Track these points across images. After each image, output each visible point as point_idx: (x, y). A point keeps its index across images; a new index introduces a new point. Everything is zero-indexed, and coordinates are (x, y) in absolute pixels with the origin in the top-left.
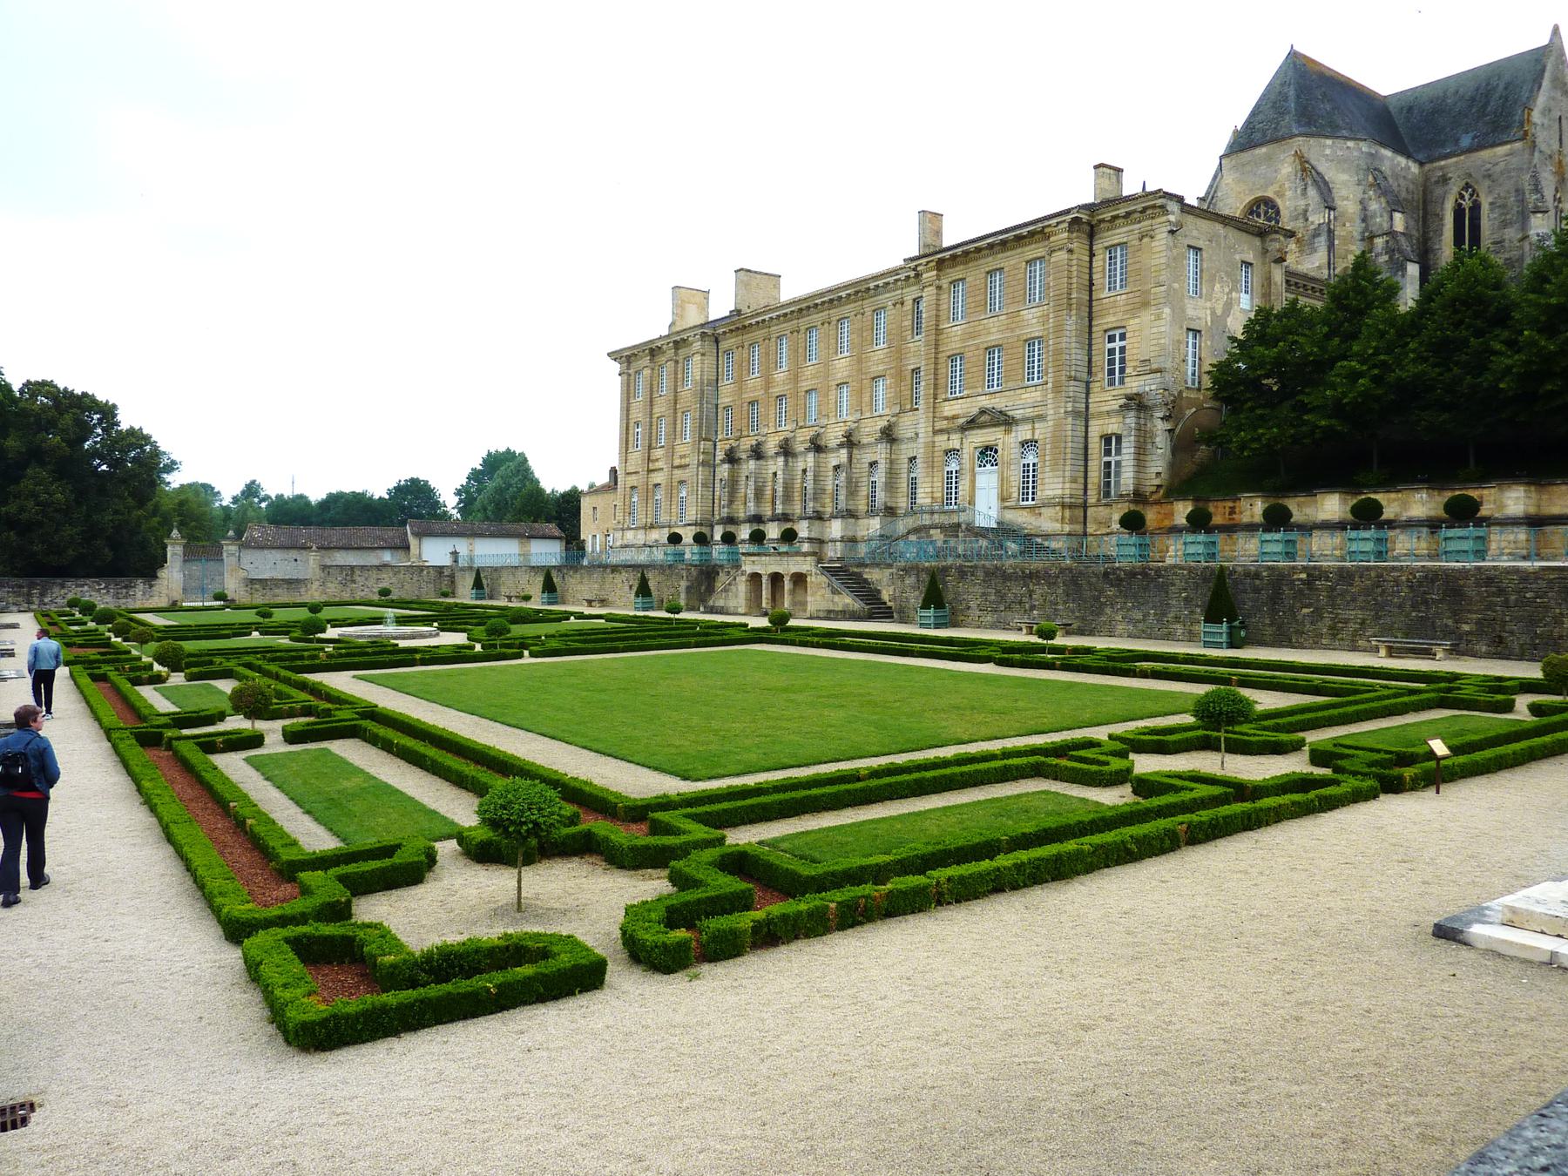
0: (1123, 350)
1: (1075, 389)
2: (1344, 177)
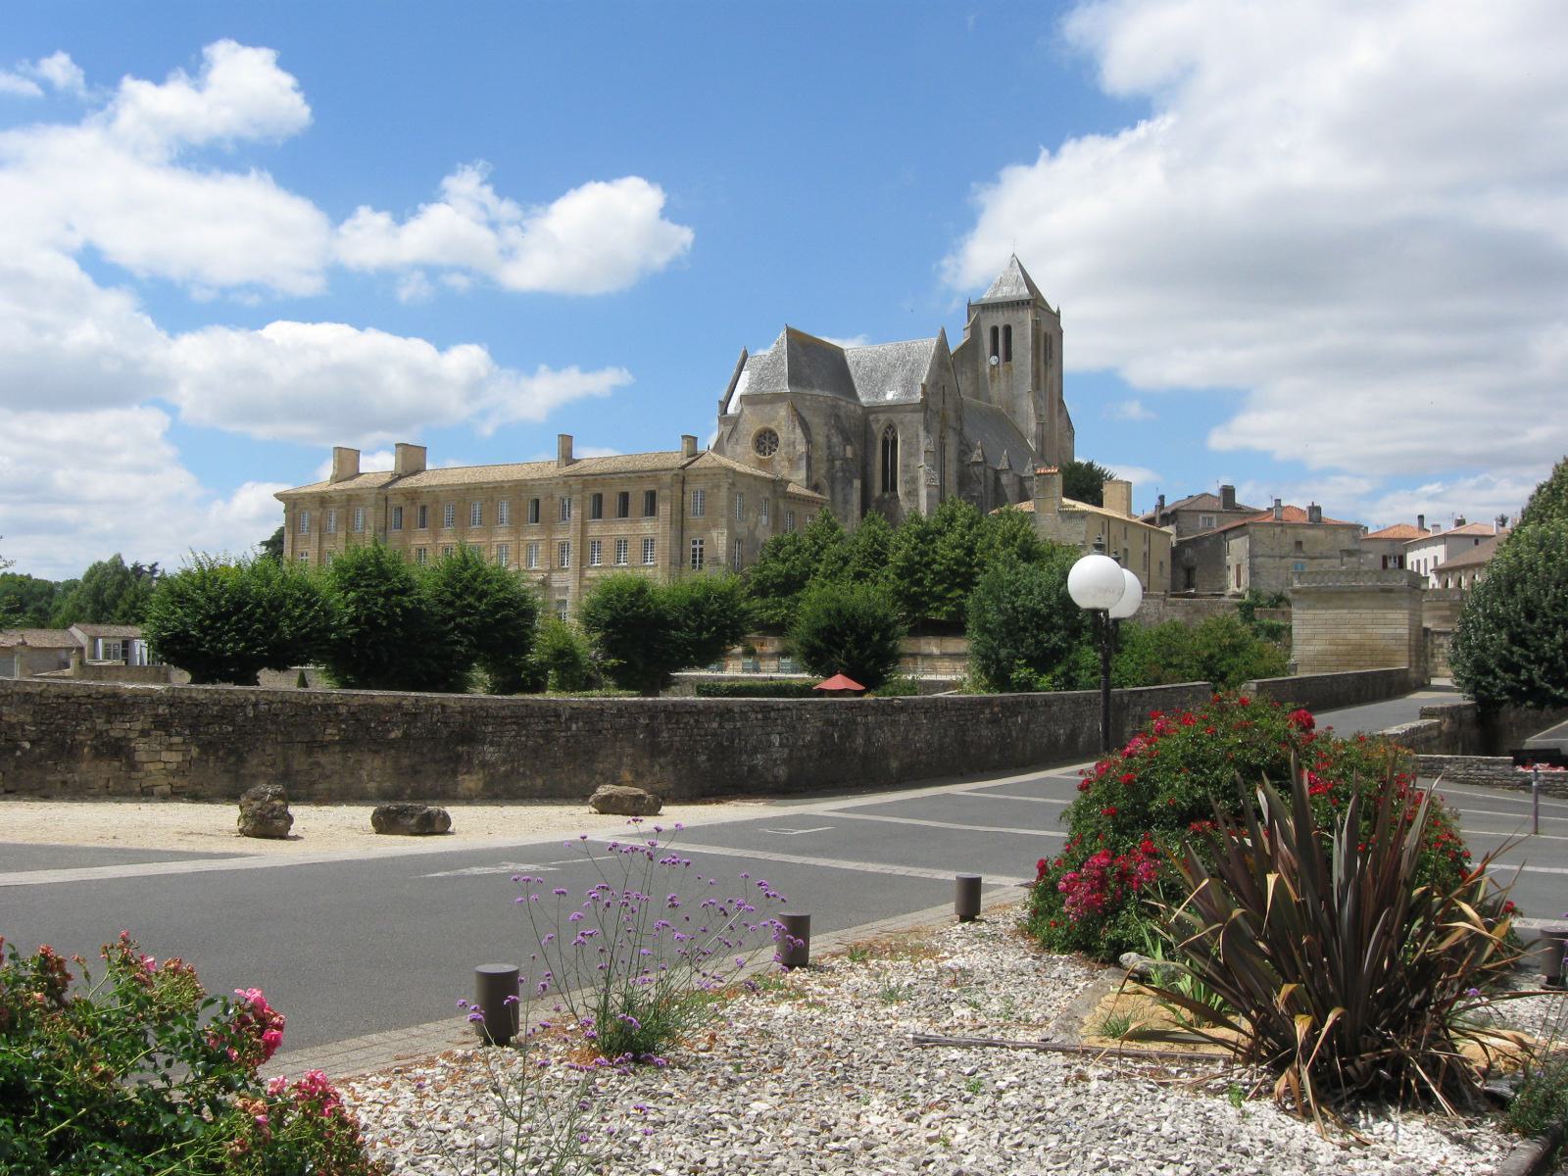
0: (701, 550)
2: (816, 420)
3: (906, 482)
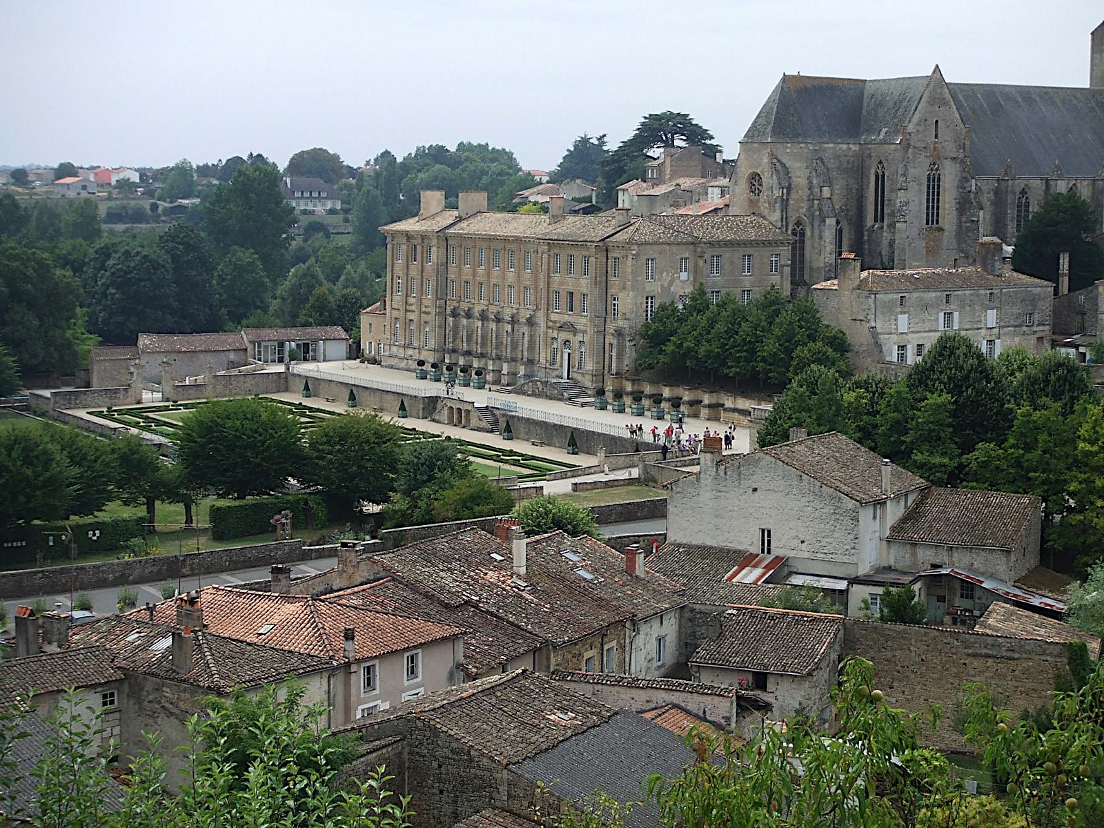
1: (599, 321)
2: (798, 165)
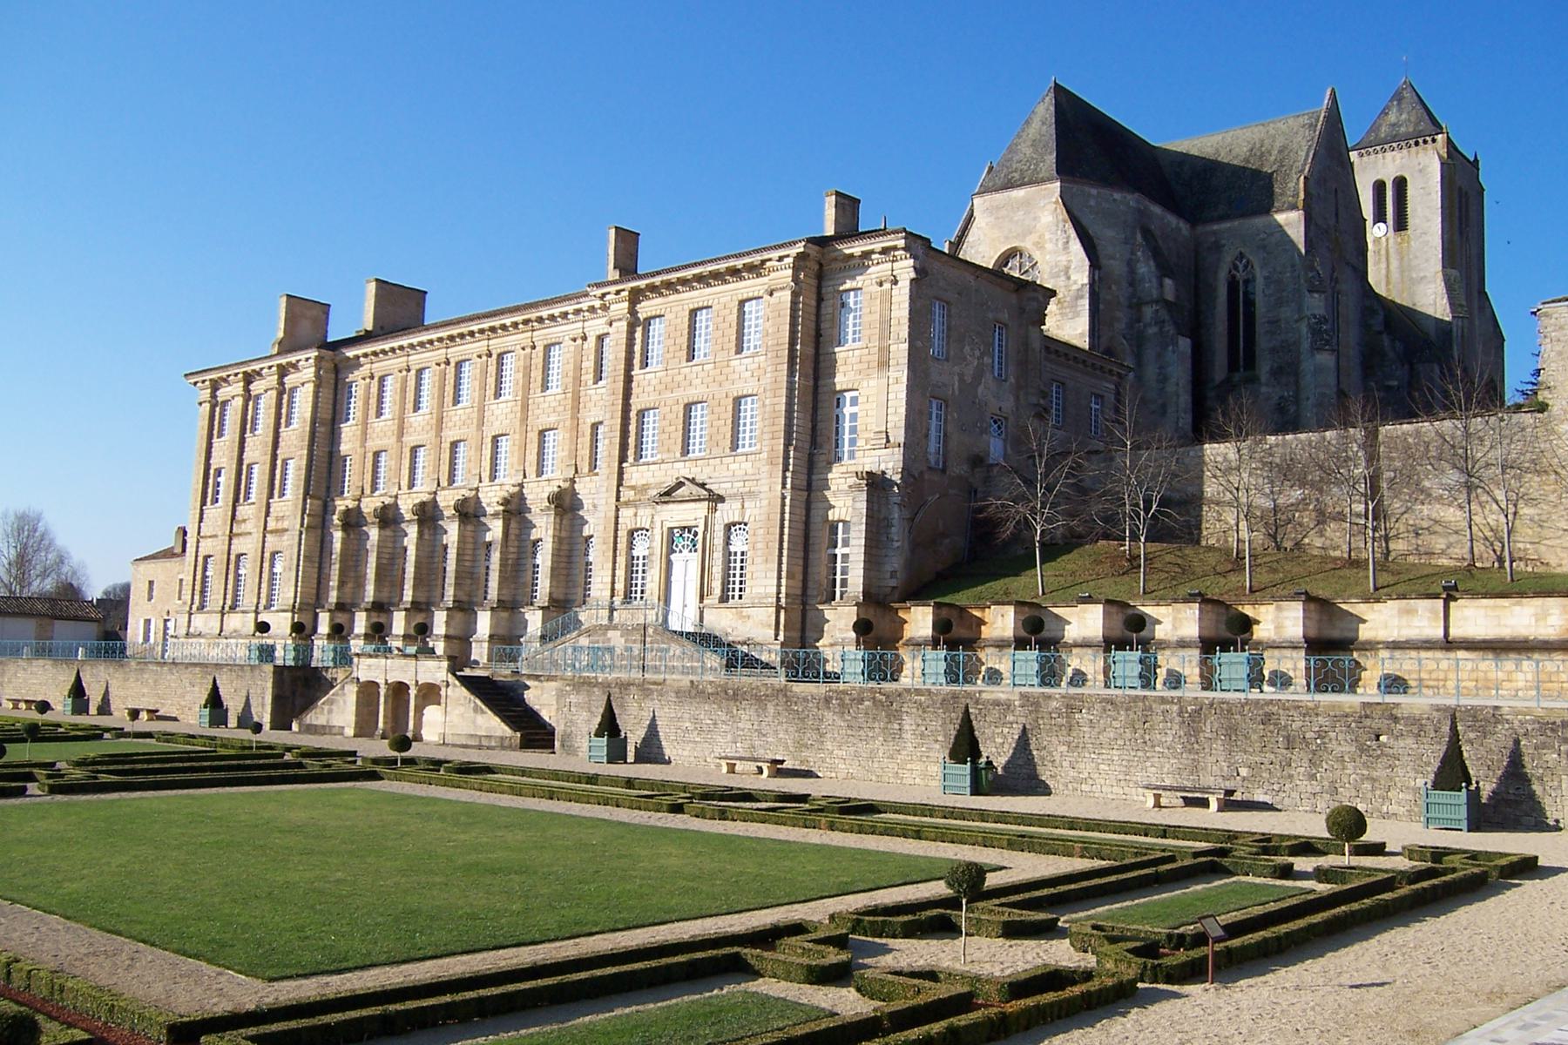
2: (1110, 233)
3: (1273, 350)
